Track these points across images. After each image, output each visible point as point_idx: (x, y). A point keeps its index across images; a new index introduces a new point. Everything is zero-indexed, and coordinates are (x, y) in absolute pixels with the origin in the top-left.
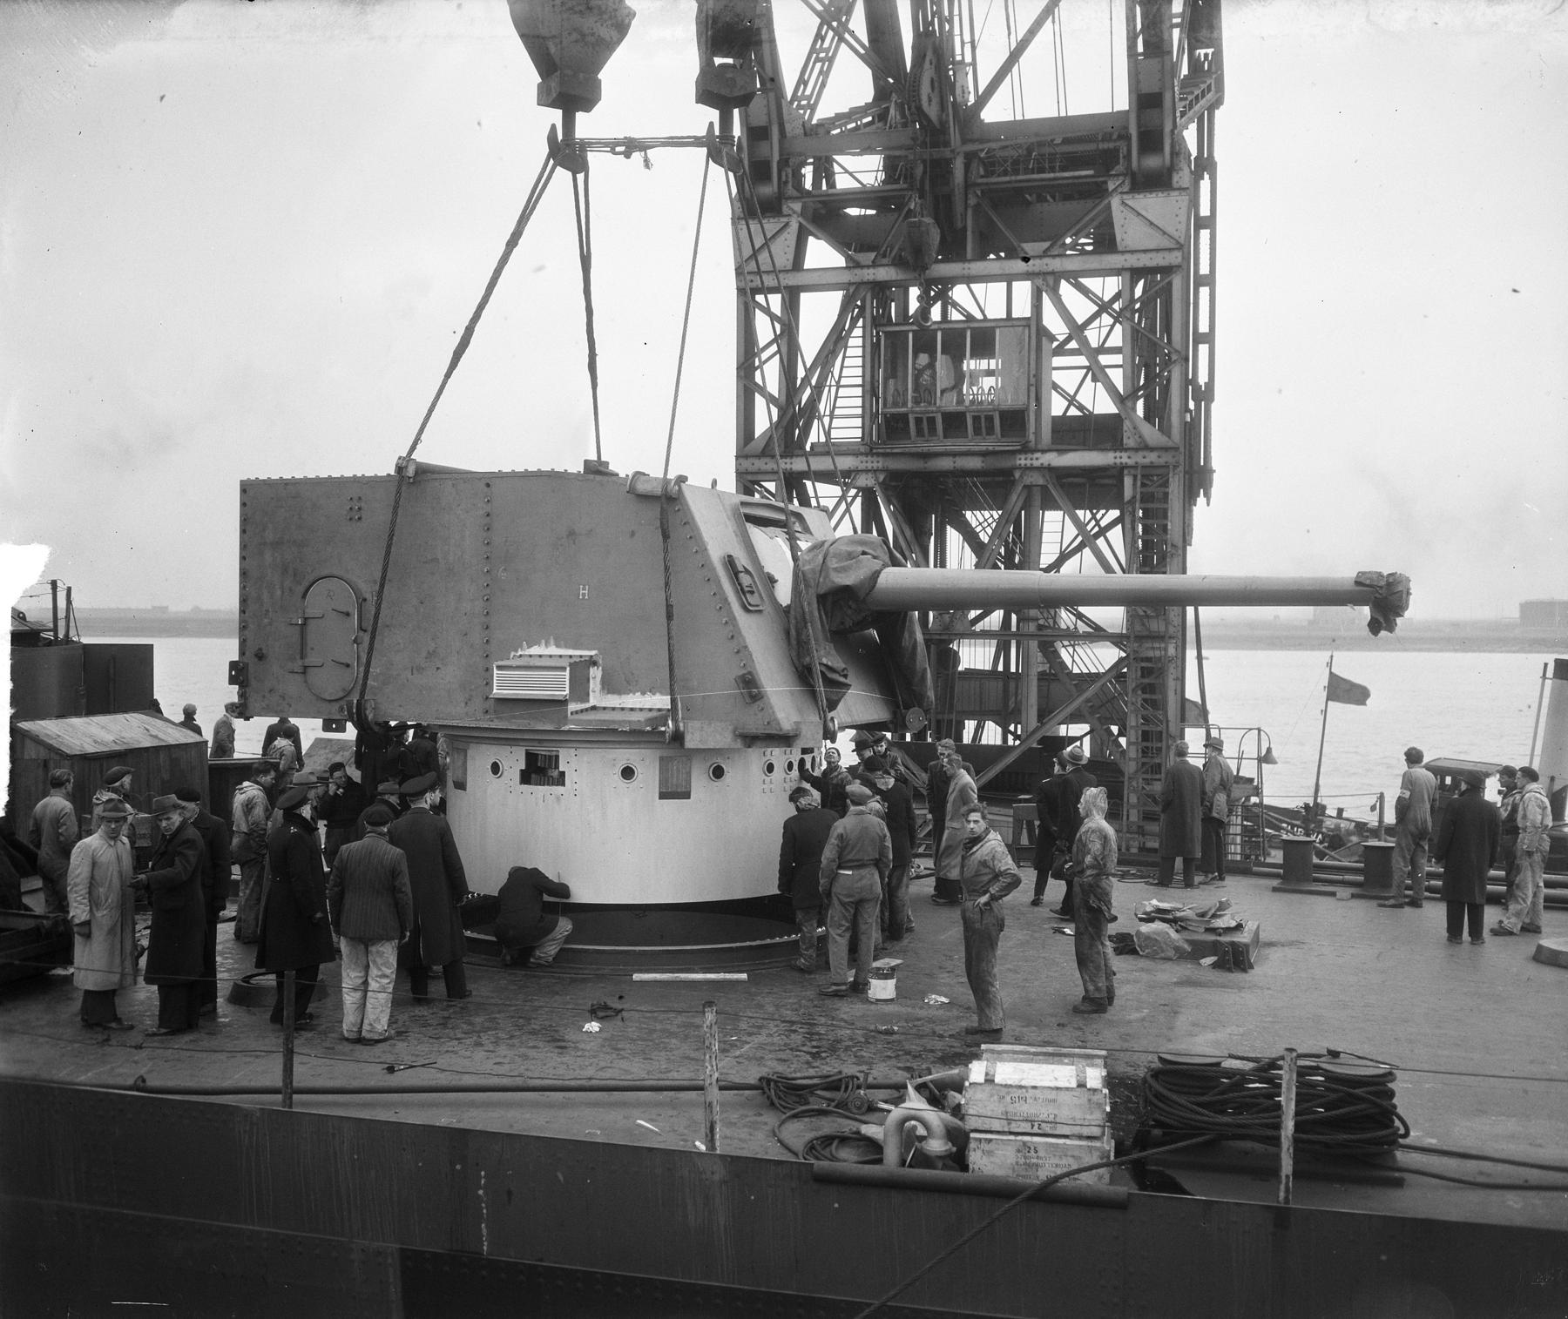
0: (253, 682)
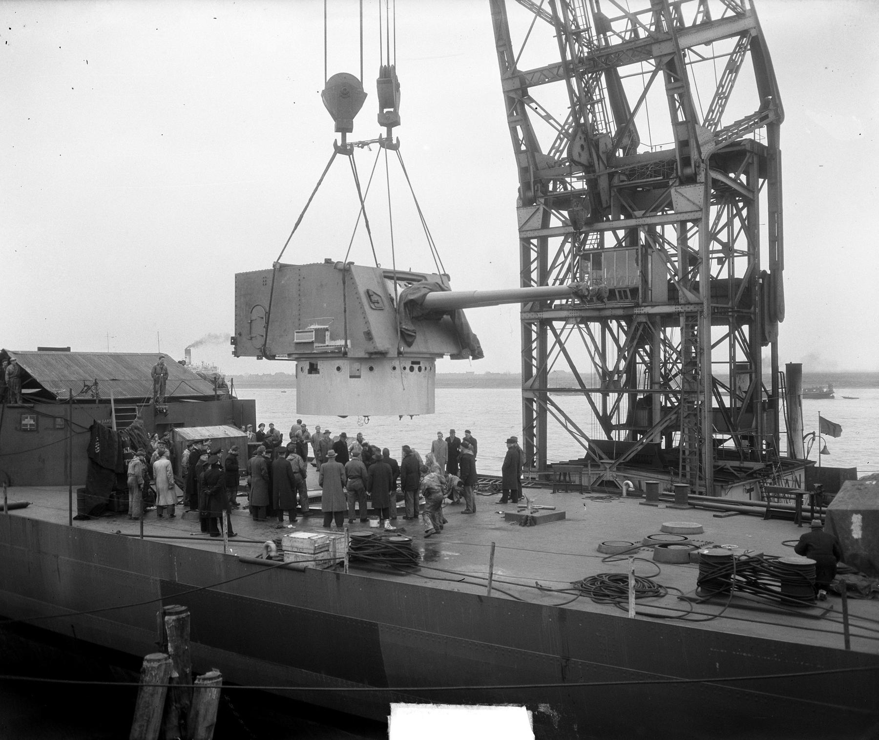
0: (238, 344)
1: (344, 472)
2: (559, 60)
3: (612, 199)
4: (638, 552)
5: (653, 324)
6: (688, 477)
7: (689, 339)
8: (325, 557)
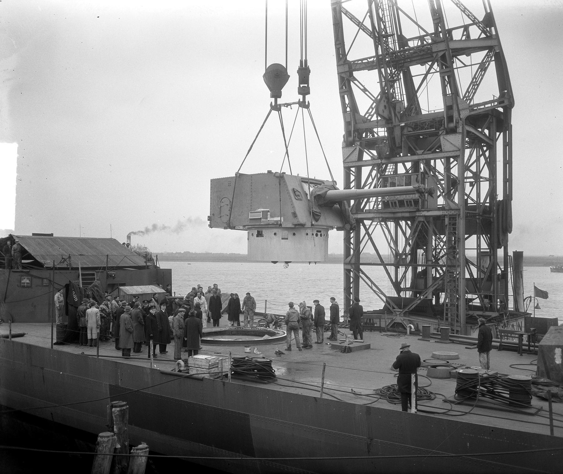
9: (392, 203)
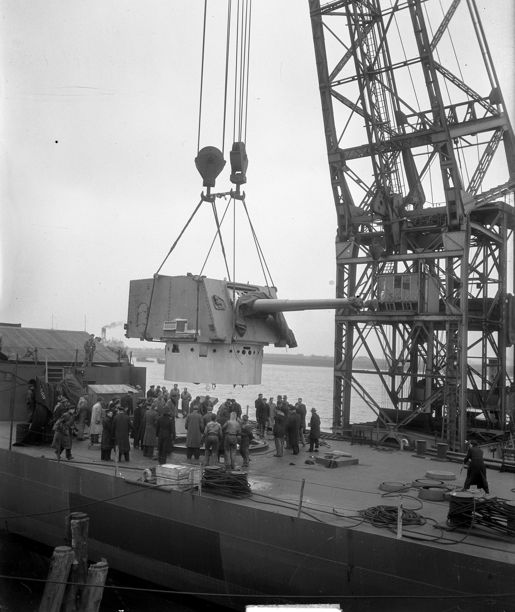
1: (202, 421)
2: (367, 142)
3: (401, 239)
4: (408, 491)
5: (427, 328)
6: (448, 438)
7: (452, 339)
8: (186, 483)
9: (388, 305)
